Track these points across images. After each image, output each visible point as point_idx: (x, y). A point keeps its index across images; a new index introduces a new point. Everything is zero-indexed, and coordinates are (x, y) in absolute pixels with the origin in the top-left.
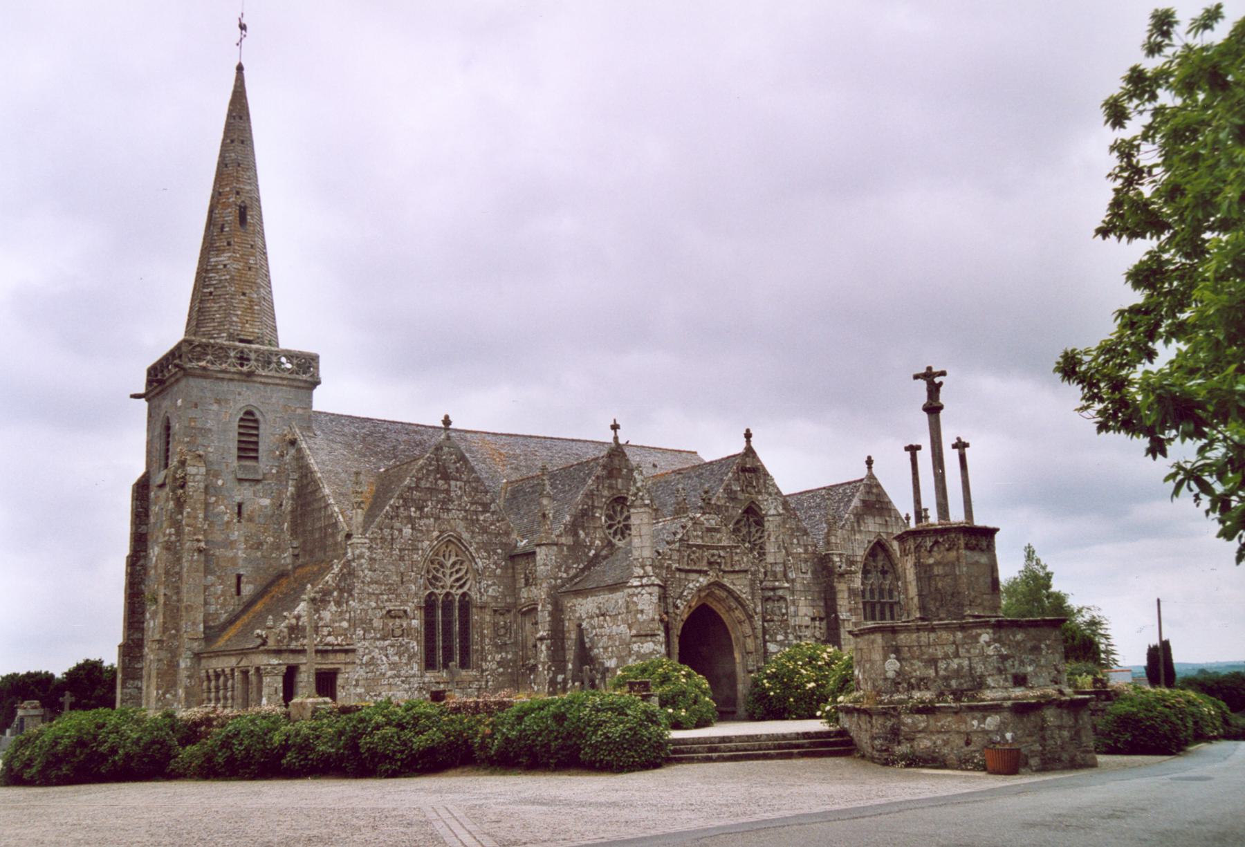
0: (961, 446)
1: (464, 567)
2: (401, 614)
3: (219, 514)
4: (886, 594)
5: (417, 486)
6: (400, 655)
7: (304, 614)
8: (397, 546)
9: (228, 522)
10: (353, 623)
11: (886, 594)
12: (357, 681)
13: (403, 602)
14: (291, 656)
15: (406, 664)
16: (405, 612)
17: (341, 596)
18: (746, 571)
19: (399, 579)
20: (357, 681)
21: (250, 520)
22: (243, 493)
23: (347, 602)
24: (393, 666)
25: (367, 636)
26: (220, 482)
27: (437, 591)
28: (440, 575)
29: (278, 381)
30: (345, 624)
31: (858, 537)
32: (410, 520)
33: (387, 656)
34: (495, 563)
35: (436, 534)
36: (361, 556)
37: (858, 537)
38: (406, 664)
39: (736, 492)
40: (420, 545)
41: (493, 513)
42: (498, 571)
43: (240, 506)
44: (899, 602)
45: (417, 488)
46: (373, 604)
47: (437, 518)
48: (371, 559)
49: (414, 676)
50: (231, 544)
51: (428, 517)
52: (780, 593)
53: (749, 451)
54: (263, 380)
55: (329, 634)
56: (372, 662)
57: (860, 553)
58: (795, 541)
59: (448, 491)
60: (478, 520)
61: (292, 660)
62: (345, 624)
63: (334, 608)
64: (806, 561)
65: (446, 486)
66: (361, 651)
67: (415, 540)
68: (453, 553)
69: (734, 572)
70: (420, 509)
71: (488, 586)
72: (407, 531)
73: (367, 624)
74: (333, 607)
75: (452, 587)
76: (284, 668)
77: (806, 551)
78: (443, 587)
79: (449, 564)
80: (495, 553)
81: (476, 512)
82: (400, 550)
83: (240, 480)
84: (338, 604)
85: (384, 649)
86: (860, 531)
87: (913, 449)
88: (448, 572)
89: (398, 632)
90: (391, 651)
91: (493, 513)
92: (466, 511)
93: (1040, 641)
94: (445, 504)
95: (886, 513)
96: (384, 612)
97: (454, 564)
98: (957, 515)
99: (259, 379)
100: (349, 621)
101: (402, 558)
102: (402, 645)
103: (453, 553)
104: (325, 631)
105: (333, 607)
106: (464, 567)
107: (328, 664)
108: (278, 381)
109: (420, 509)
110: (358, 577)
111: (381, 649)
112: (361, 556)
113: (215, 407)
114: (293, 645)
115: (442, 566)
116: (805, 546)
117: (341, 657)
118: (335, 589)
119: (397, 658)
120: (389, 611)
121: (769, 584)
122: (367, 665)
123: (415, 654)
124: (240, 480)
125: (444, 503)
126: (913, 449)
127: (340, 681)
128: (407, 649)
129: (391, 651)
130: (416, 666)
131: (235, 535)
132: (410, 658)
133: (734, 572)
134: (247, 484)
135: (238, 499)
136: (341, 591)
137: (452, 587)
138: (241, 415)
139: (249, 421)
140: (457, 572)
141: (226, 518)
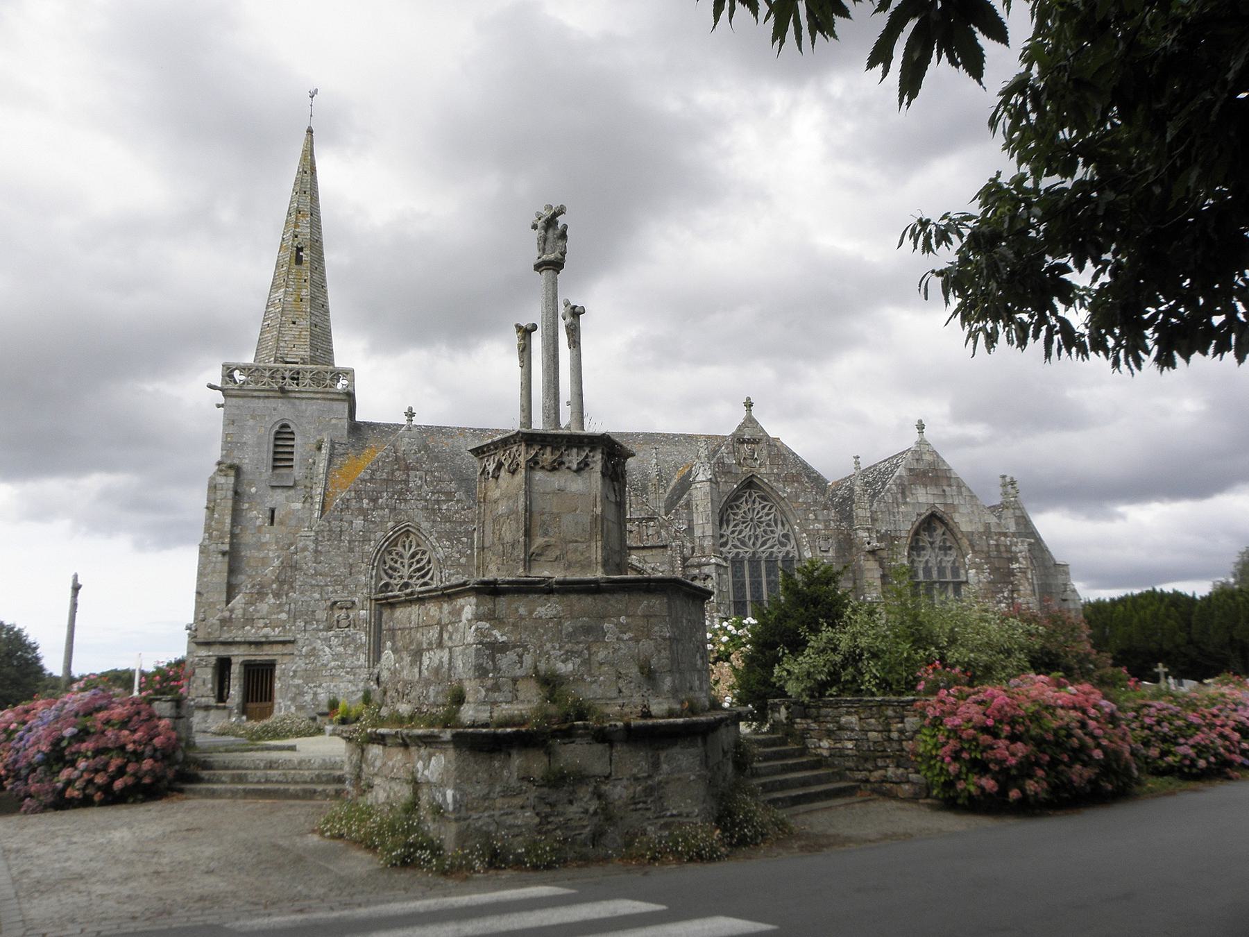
0: (576, 313)
1: (426, 557)
2: (349, 605)
3: (251, 519)
4: (948, 573)
5: (372, 478)
6: (346, 646)
7: (239, 606)
8: (346, 538)
9: (260, 527)
10: (294, 617)
11: (948, 573)
12: (295, 672)
13: (351, 593)
14: (222, 648)
15: (352, 655)
16: (353, 603)
17: (280, 588)
18: (665, 547)
19: (347, 571)
20: (295, 672)
21: (281, 523)
22: (278, 498)
23: (287, 595)
24: (337, 656)
25: (308, 627)
26: (253, 490)
27: (392, 581)
28: (398, 565)
29: (312, 395)
30: (284, 616)
31: (903, 508)
32: (363, 513)
33: (330, 647)
34: (459, 552)
35: (390, 524)
36: (305, 549)
37: (903, 508)
38: (352, 655)
39: (730, 466)
40: (372, 536)
41: (458, 501)
42: (463, 560)
43: (273, 511)
44: (967, 582)
45: (371, 479)
46: (317, 596)
47: (393, 509)
48: (316, 551)
49: (360, 667)
50: (260, 546)
51: (382, 509)
52: (706, 570)
53: (750, 421)
54: (297, 395)
55: (266, 626)
56: (313, 653)
57: (906, 528)
58: (811, 516)
59: (406, 482)
60: (440, 509)
61: (222, 652)
62: (284, 616)
63: (272, 601)
64: (827, 539)
65: (404, 477)
66: (300, 643)
67: (367, 531)
68: (414, 543)
69: (644, 548)
70: (375, 500)
71: (450, 575)
72: (359, 522)
73: (309, 616)
74: (271, 600)
75: (411, 577)
76: (213, 660)
77: (827, 527)
78: (401, 577)
79: (408, 554)
80: (459, 541)
81: (438, 502)
82: (349, 542)
83: (273, 487)
84: (277, 595)
85: (327, 640)
86: (905, 503)
87: (526, 332)
88: (406, 561)
89: (344, 623)
90: (334, 641)
91: (458, 501)
92: (426, 501)
93: (603, 618)
94: (402, 496)
95: (945, 482)
96: (329, 603)
97: (413, 556)
98: (538, 425)
99: (293, 395)
100: (289, 612)
101: (351, 550)
102: (348, 636)
103: (414, 543)
104: (261, 623)
105: (271, 600)
106: (426, 557)
107: (262, 655)
108: (312, 395)
109: (375, 500)
110: (301, 569)
111: (325, 639)
112: (305, 549)
113: (251, 422)
114: (225, 637)
115: (401, 556)
116: (825, 521)
117: (278, 649)
118: (273, 582)
119: (341, 649)
120: (335, 603)
121: (694, 561)
122: (307, 656)
123: (362, 645)
124: (273, 487)
125: (401, 493)
126: (526, 332)
127: (277, 673)
128: (354, 640)
129: (334, 641)
130: (363, 657)
131: (267, 537)
132: (357, 649)
133: (644, 548)
134: (279, 491)
135: (269, 505)
136: (282, 583)
137: (411, 577)
138: (277, 428)
139: (283, 434)
140: (418, 562)
141: (258, 522)
